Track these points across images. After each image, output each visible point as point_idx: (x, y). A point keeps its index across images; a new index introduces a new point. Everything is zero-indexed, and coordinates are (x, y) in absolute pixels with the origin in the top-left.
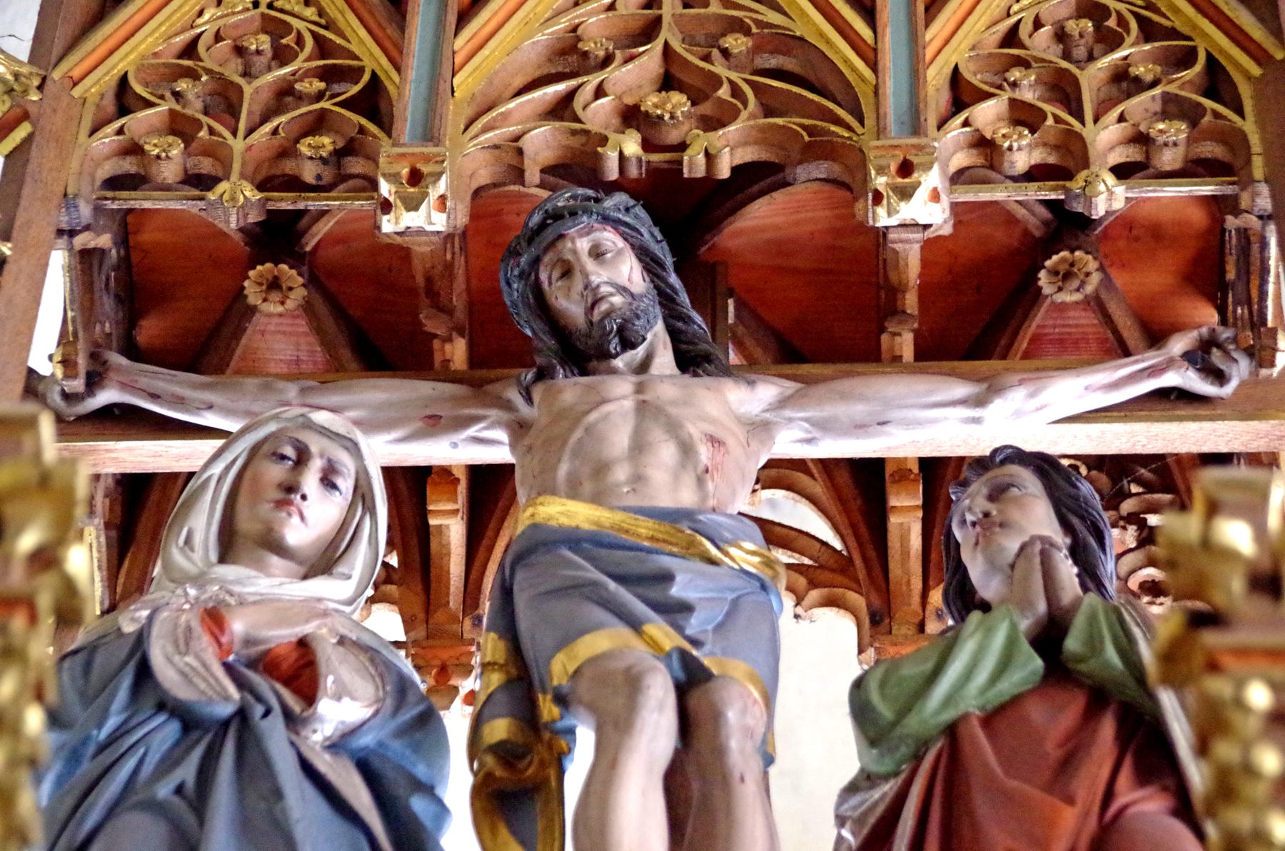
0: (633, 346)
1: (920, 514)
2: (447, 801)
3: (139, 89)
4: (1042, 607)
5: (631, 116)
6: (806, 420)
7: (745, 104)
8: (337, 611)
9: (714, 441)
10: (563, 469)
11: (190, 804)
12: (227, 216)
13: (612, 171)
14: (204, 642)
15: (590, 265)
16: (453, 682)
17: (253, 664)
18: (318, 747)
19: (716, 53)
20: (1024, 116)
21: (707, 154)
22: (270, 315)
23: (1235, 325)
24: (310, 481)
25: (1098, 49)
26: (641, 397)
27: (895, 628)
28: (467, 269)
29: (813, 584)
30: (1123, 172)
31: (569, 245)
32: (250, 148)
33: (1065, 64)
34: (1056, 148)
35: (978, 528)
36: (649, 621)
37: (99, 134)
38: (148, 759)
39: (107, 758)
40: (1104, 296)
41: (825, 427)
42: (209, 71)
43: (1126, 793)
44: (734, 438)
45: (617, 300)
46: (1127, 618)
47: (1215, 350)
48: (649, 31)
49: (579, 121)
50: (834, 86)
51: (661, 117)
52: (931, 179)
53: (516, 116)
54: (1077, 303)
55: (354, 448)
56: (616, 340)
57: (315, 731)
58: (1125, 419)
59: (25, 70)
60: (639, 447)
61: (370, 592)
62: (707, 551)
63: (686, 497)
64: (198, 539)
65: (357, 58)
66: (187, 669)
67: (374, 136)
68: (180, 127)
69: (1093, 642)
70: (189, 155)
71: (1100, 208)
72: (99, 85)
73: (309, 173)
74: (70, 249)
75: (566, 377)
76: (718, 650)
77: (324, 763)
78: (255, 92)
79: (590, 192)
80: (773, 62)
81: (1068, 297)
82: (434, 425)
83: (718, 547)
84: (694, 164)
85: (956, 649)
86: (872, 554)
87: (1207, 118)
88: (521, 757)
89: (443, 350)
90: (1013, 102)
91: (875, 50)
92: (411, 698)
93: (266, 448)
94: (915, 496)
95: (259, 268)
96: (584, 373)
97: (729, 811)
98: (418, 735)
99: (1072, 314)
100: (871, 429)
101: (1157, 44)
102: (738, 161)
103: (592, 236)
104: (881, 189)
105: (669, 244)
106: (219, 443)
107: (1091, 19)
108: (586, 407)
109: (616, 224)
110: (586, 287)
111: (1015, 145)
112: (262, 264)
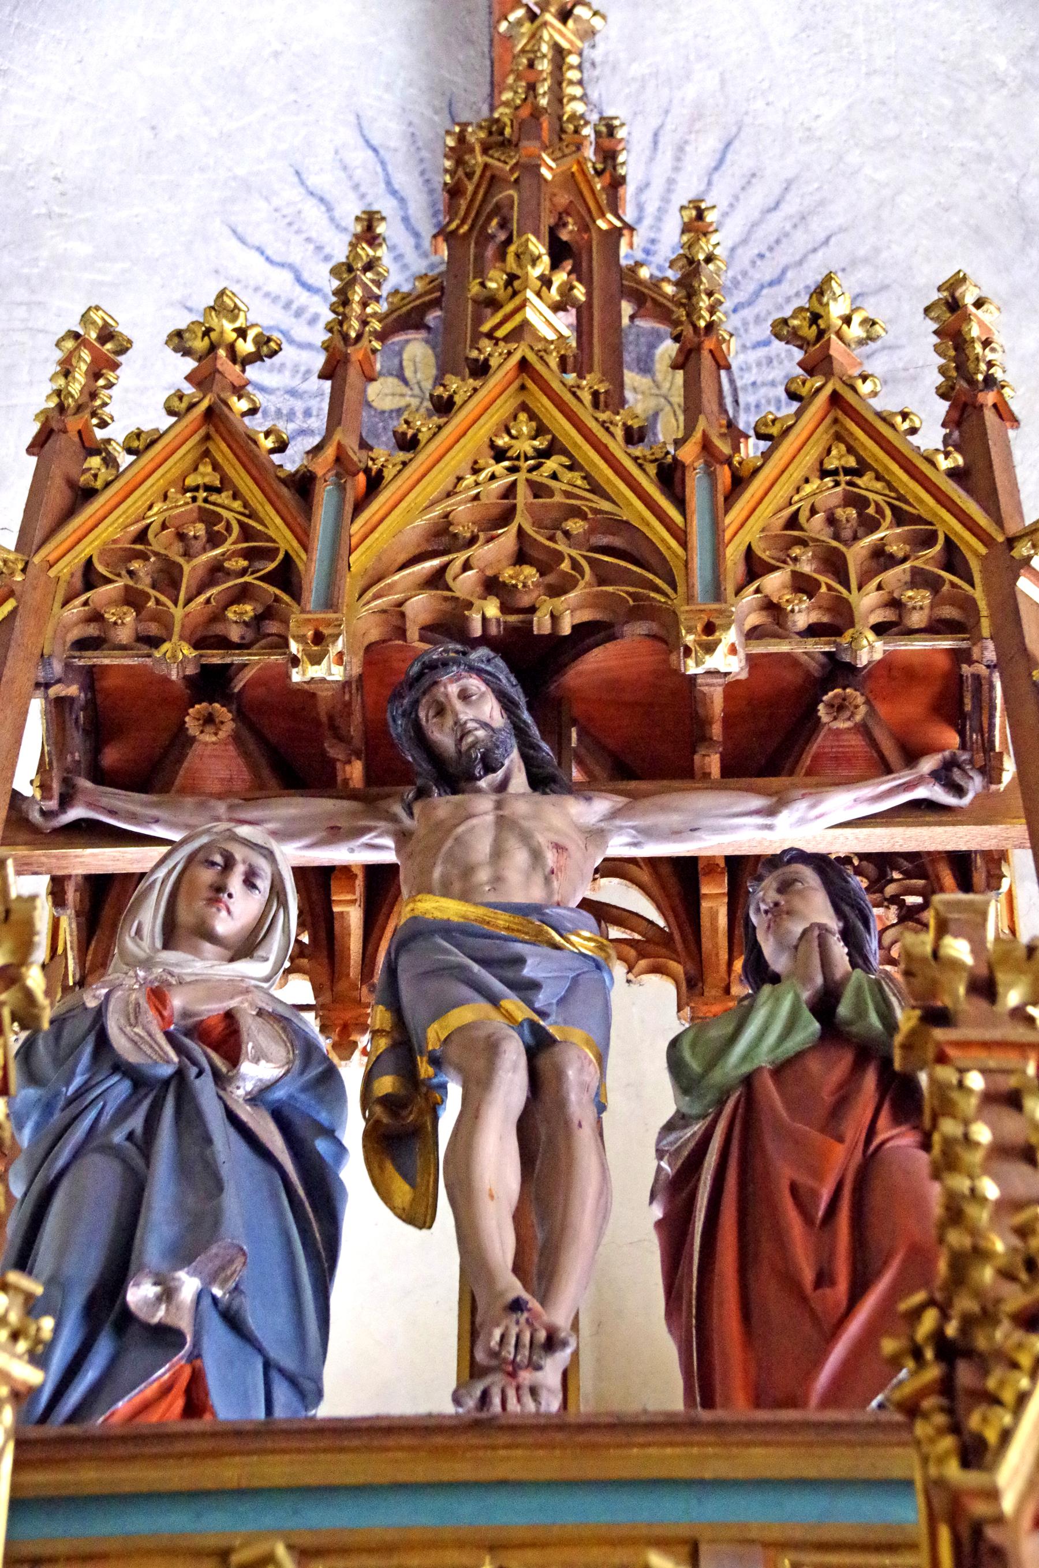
0: (494, 770)
1: (726, 900)
2: (345, 1142)
3: (101, 569)
4: (819, 980)
5: (492, 586)
6: (633, 827)
7: (582, 574)
8: (257, 987)
9: (558, 847)
10: (437, 873)
11: (138, 1147)
12: (169, 669)
13: (476, 630)
14: (150, 1016)
15: (458, 705)
16: (352, 1038)
17: (188, 1033)
18: (241, 1100)
19: (559, 534)
20: (803, 585)
21: (552, 616)
22: (206, 744)
23: (972, 750)
24: (235, 883)
25: (861, 531)
26: (501, 813)
27: (706, 990)
28: (363, 707)
29: (642, 955)
30: (880, 629)
31: (442, 689)
32: (187, 615)
33: (835, 544)
34: (828, 610)
35: (770, 916)
36: (506, 997)
37: (69, 606)
38: (107, 1108)
39: (74, 1109)
40: (871, 723)
41: (649, 833)
42: (156, 554)
43: (885, 1131)
44: (575, 843)
45: (481, 733)
46: (887, 989)
47: (955, 770)
48: (506, 517)
49: (450, 589)
50: (653, 560)
51: (515, 586)
52: (730, 636)
53: (400, 587)
54: (849, 729)
55: (269, 855)
56: (480, 766)
57: (238, 1088)
58: (886, 825)
59: (11, 557)
60: (498, 853)
61: (287, 964)
62: (552, 938)
63: (536, 894)
64: (146, 931)
65: (274, 541)
66: (136, 1038)
67: (287, 604)
68: (133, 599)
69: (860, 1012)
70: (140, 621)
71: (863, 659)
72: (68, 567)
73: (235, 634)
74: (46, 698)
75: (440, 795)
76: (560, 1020)
77: (246, 1113)
78: (192, 569)
79: (459, 647)
80: (605, 540)
81: (842, 725)
82: (335, 835)
83: (561, 935)
84: (541, 624)
85: (752, 1016)
86: (688, 930)
87: (946, 588)
88: (404, 1106)
89: (344, 771)
90: (795, 574)
91: (685, 532)
92: (316, 1058)
93: (201, 856)
94: (721, 886)
95: (197, 706)
96: (455, 792)
97: (569, 1148)
98: (321, 1089)
99: (845, 737)
100: (684, 835)
101: (906, 528)
102: (577, 621)
103: (461, 682)
104: (690, 644)
105: (523, 687)
106: (164, 850)
107: (854, 507)
108: (457, 821)
109: (479, 672)
110: (456, 723)
111: (797, 608)
112: (200, 703)
